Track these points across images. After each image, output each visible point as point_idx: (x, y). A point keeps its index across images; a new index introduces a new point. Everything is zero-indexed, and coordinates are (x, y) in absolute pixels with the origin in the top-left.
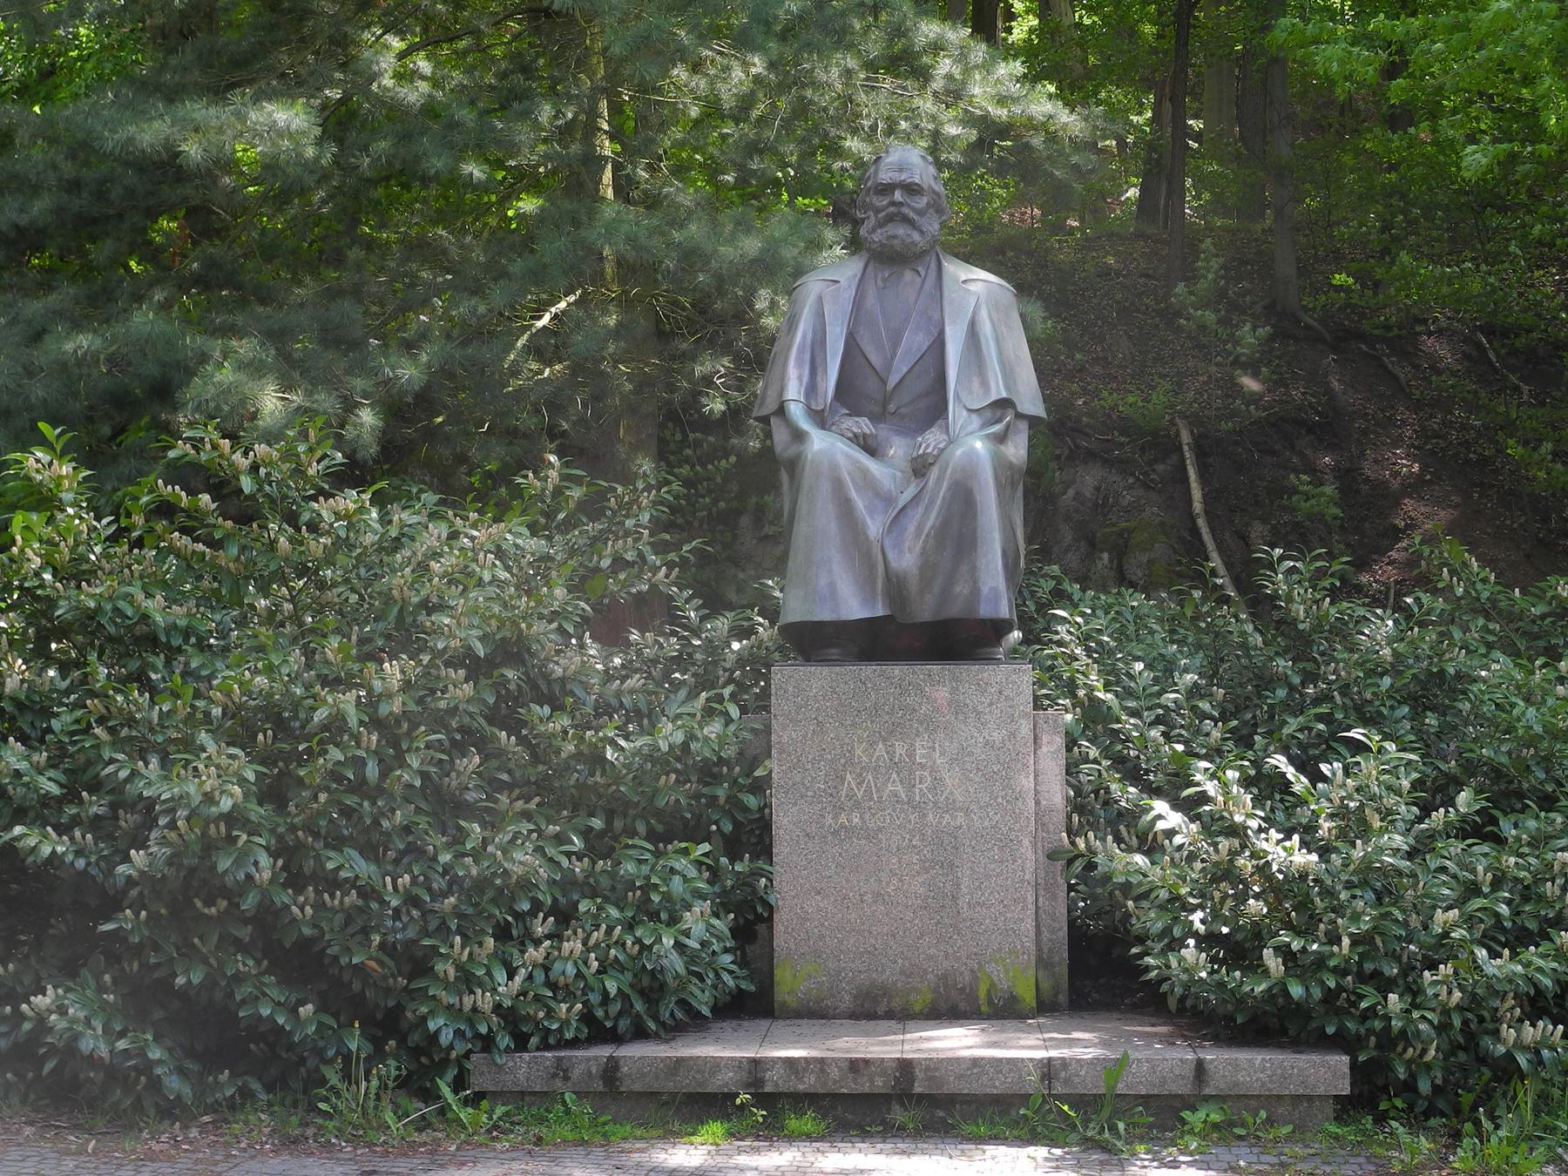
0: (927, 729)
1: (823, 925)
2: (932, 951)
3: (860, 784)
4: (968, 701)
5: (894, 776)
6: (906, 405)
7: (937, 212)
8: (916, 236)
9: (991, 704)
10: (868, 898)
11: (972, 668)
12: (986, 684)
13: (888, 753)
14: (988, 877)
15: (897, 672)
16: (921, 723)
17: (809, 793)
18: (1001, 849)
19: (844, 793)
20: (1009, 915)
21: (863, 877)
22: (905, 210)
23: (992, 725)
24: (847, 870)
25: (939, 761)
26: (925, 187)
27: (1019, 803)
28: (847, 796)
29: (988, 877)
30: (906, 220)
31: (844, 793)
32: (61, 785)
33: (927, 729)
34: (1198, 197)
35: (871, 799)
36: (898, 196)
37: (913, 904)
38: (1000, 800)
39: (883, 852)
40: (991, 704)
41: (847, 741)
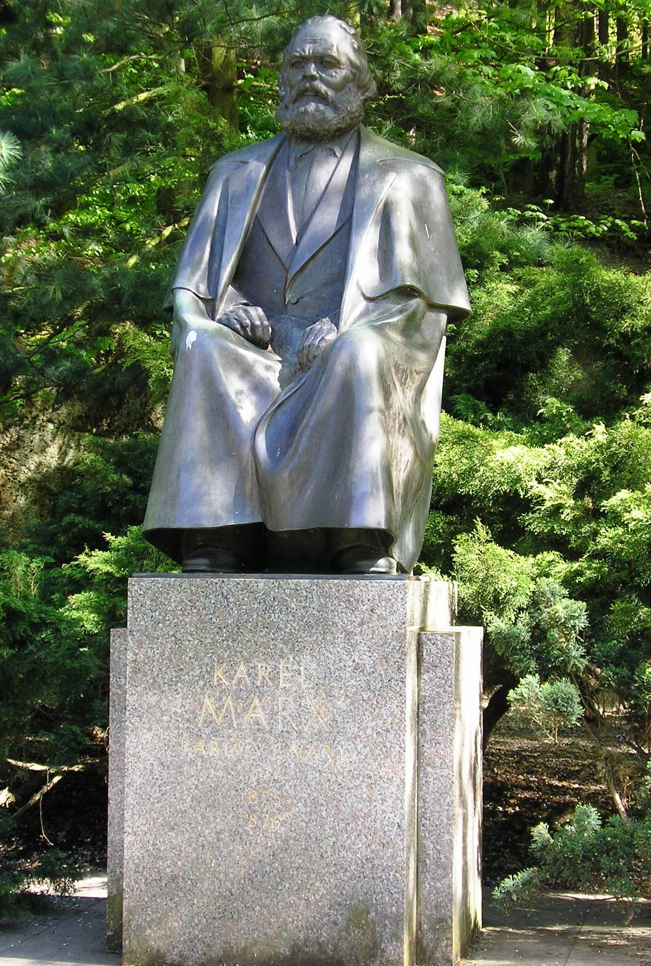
0: (292, 650)
1: (175, 865)
2: (293, 899)
3: (219, 709)
4: (337, 620)
5: (256, 701)
6: (309, 294)
7: (359, 87)
8: (330, 114)
9: (361, 624)
10: (225, 836)
11: (343, 582)
12: (357, 601)
13: (249, 675)
14: (355, 817)
15: (261, 585)
16: (285, 643)
17: (165, 718)
18: (370, 786)
19: (201, 719)
20: (376, 862)
21: (219, 813)
22: (318, 84)
23: (362, 648)
24: (203, 805)
25: (304, 686)
26: (343, 60)
27: (391, 736)
28: (205, 721)
29: (355, 817)
30: (320, 97)
31: (201, 719)
32: (493, 895)
33: (292, 650)
34: (124, 363)
35: (230, 726)
36: (313, 70)
37: (273, 845)
38: (369, 732)
39: (242, 786)
40: (361, 624)
41: (206, 660)
